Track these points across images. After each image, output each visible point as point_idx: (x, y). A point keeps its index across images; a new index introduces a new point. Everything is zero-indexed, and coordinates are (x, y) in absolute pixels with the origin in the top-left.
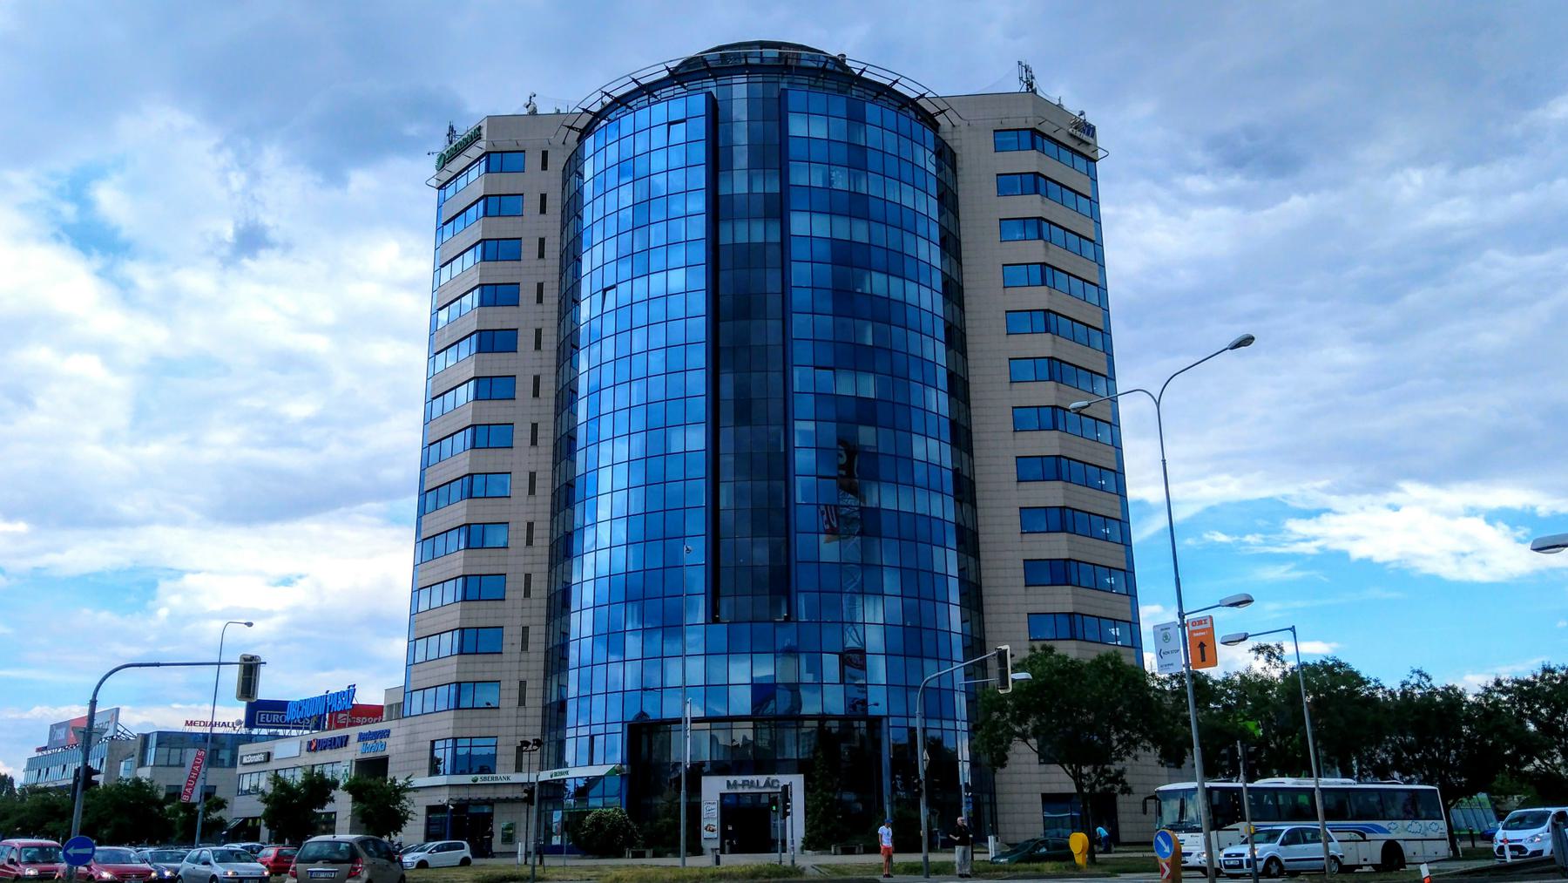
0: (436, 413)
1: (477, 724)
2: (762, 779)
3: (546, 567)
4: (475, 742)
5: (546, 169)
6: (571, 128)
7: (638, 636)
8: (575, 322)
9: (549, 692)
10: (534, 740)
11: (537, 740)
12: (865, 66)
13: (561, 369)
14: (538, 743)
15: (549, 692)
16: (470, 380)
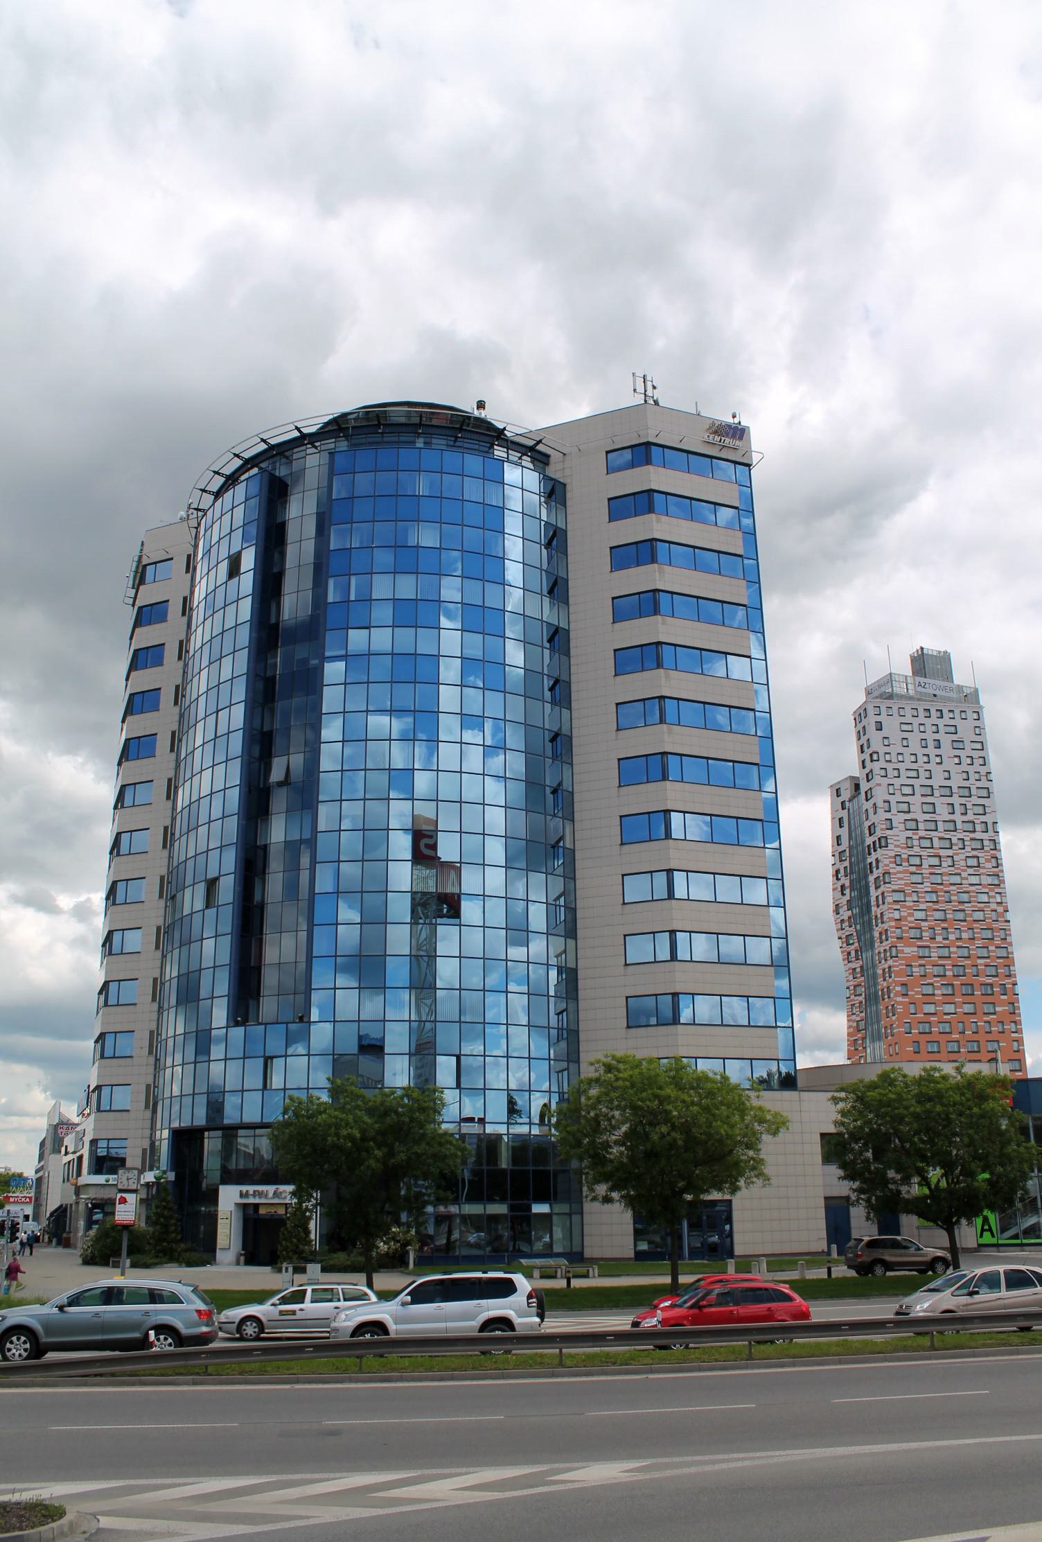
1: (114, 1124)
2: (270, 1189)
4: (112, 1144)
6: (217, 473)
7: (409, 834)
12: (505, 425)
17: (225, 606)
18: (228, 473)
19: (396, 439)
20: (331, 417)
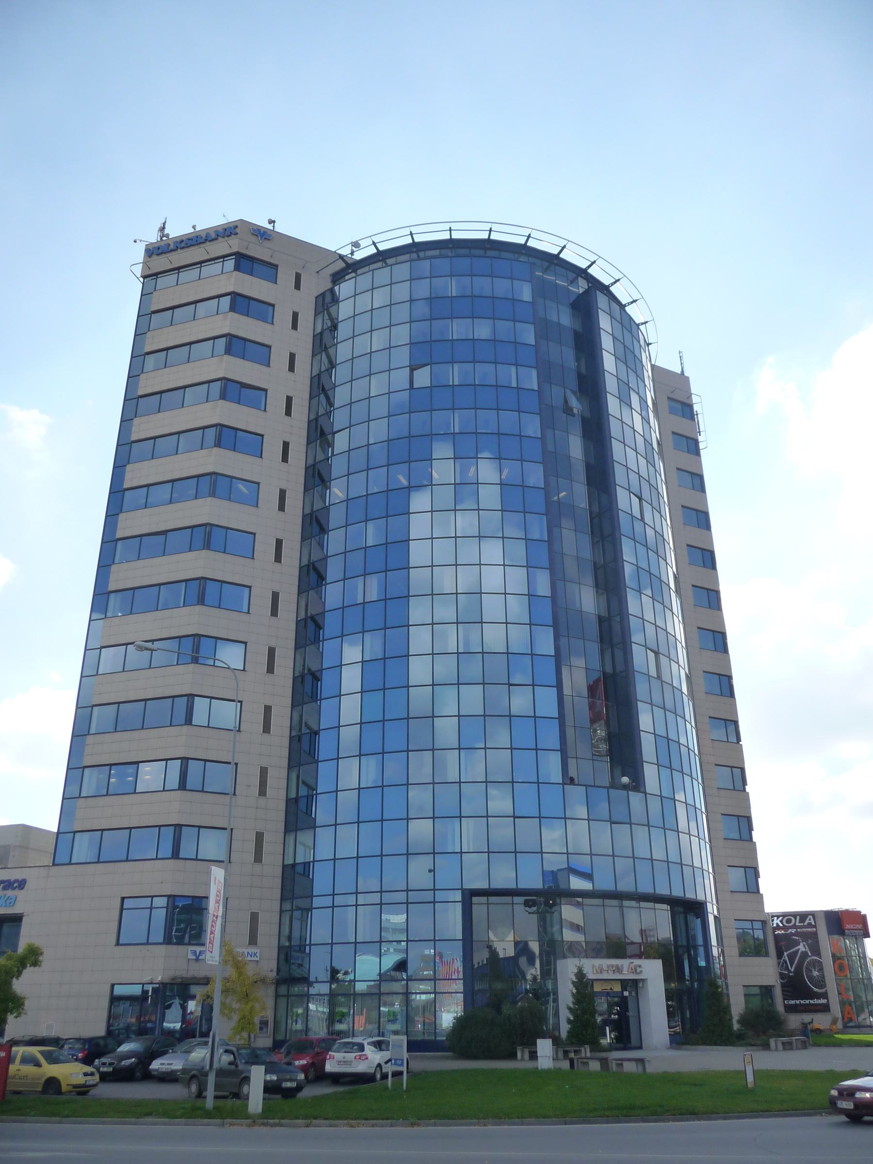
6: (374, 244)
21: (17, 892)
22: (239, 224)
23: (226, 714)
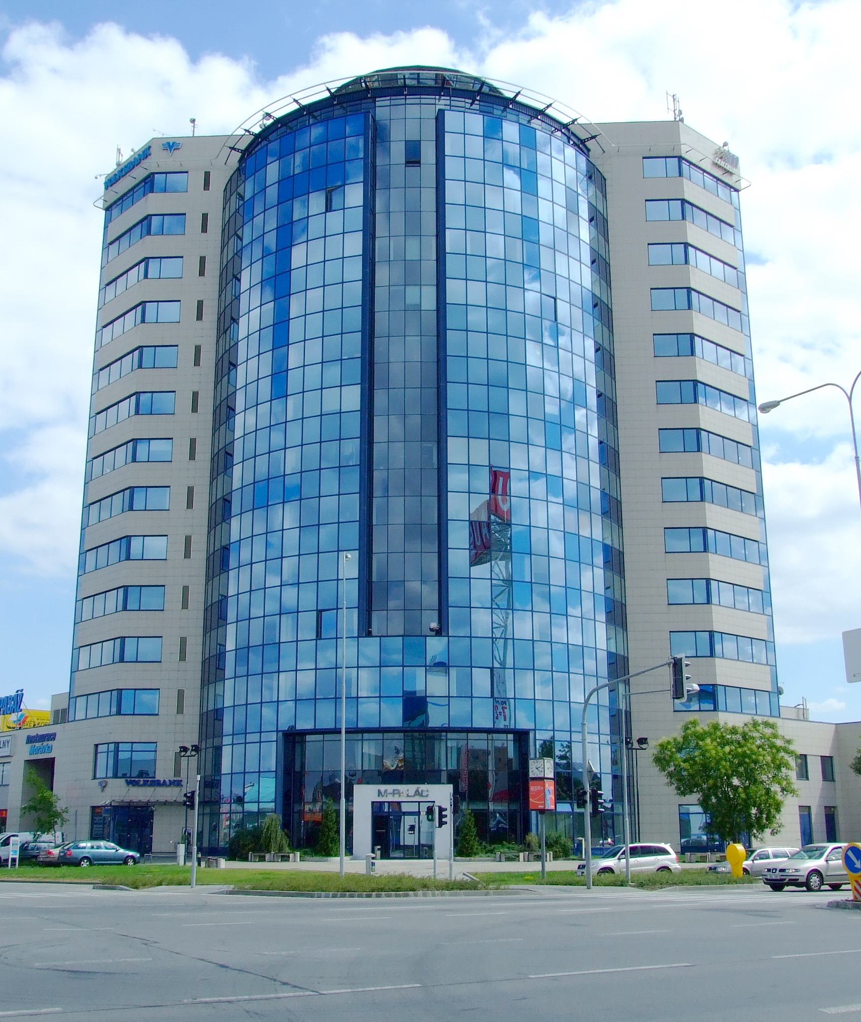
0: (100, 426)
3: (203, 580)
5: (186, 537)
6: (233, 148)
8: (232, 383)
9: (205, 701)
10: (192, 746)
11: (195, 746)
13: (215, 481)
14: (196, 748)
15: (205, 701)
16: (131, 396)
17: (249, 311)
18: (243, 148)
19: (418, 101)
20: (355, 78)
21: (50, 743)
22: (149, 145)
23: (156, 547)
